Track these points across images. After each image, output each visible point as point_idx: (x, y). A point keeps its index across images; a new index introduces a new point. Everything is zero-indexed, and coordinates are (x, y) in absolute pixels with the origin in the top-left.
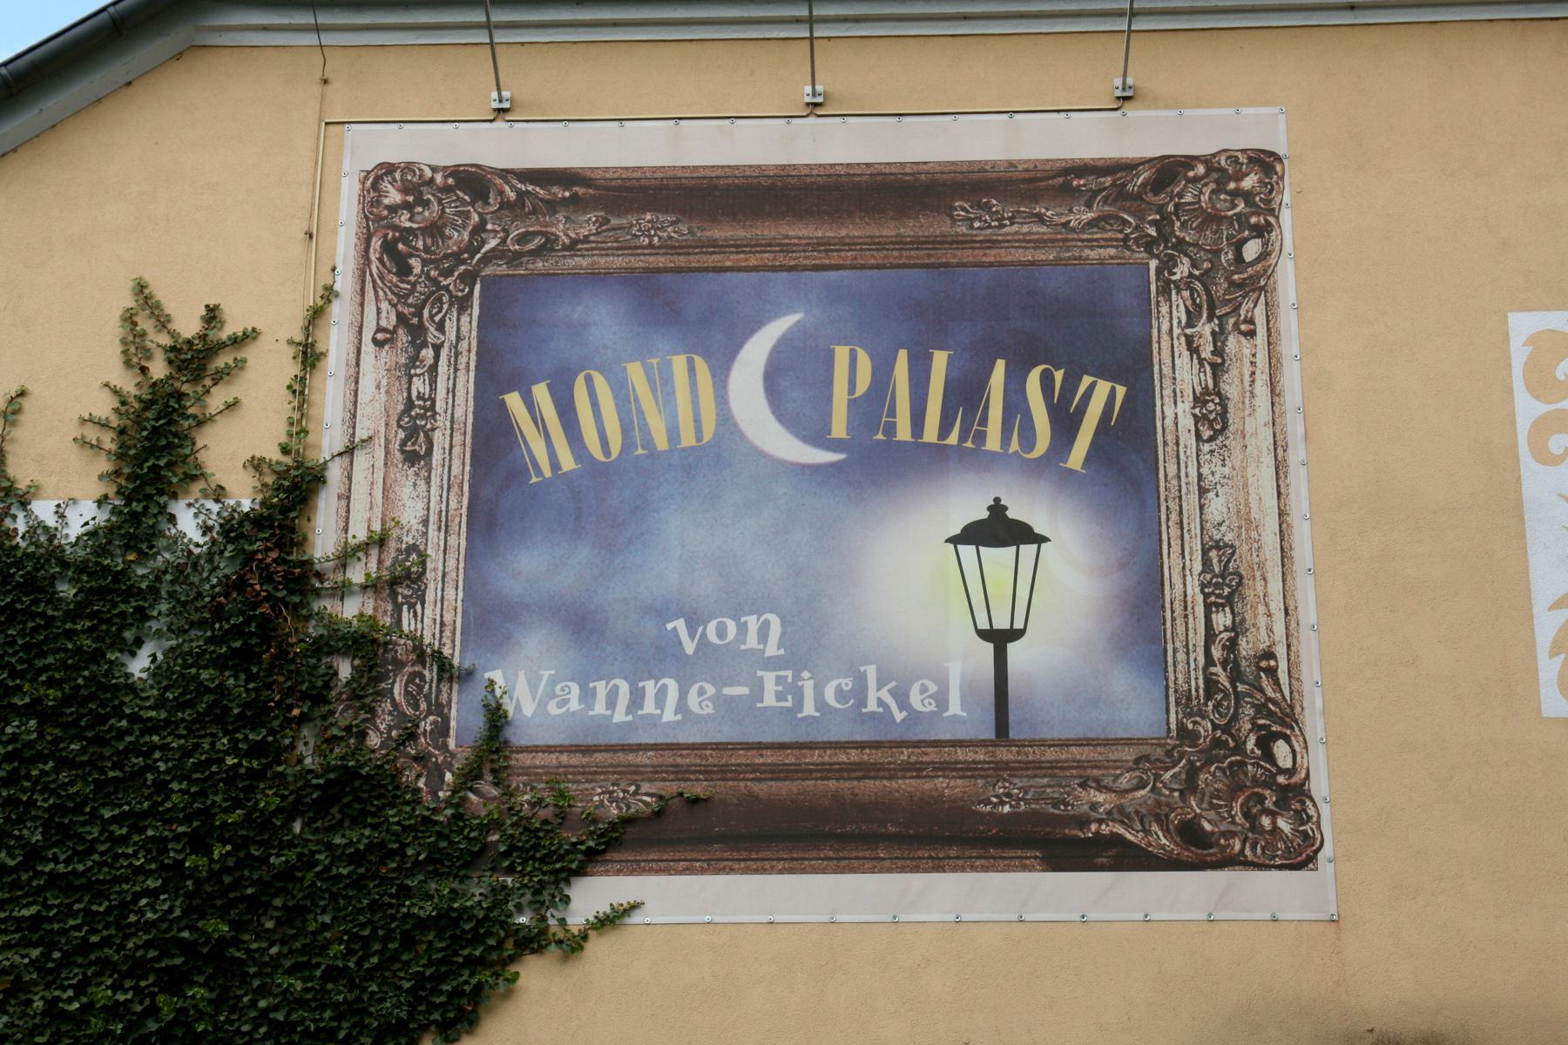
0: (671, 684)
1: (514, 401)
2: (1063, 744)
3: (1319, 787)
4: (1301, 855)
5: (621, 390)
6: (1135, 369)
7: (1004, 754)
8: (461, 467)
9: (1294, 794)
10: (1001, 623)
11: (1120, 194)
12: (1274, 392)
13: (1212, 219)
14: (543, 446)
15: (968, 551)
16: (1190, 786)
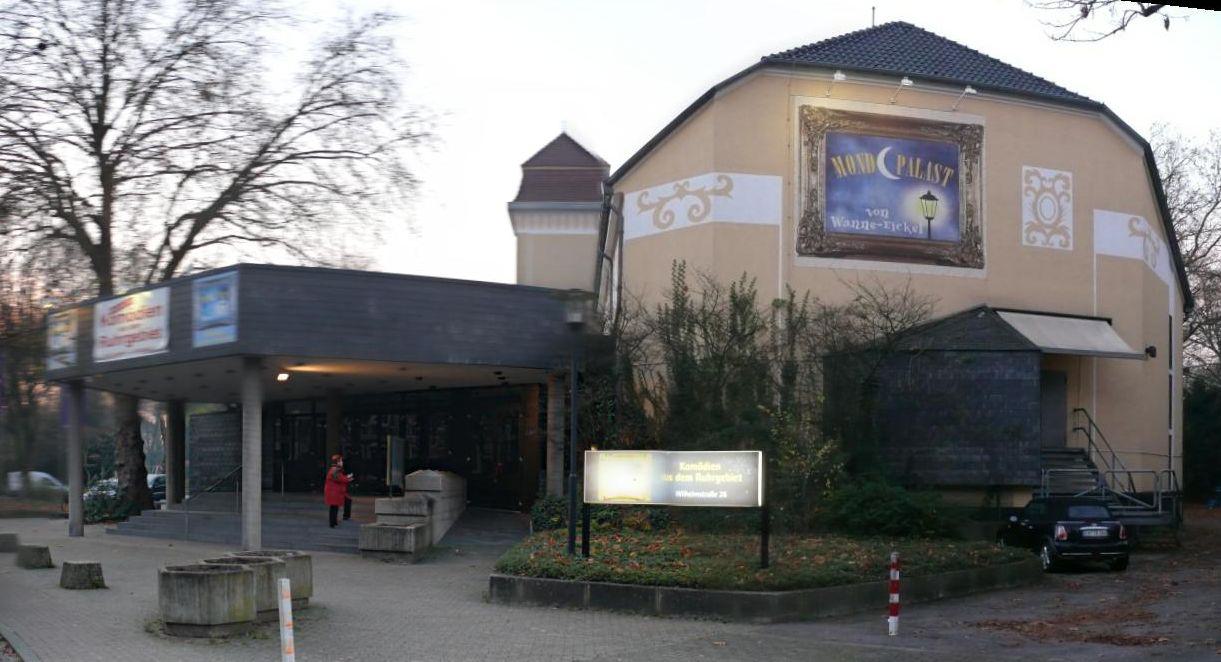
0: (867, 223)
1: (834, 160)
2: (941, 241)
3: (985, 254)
4: (981, 266)
5: (855, 159)
6: (955, 167)
7: (930, 242)
8: (823, 173)
9: (980, 255)
10: (930, 216)
11: (953, 130)
12: (981, 176)
13: (970, 138)
14: (840, 171)
15: (924, 201)
16: (963, 251)
